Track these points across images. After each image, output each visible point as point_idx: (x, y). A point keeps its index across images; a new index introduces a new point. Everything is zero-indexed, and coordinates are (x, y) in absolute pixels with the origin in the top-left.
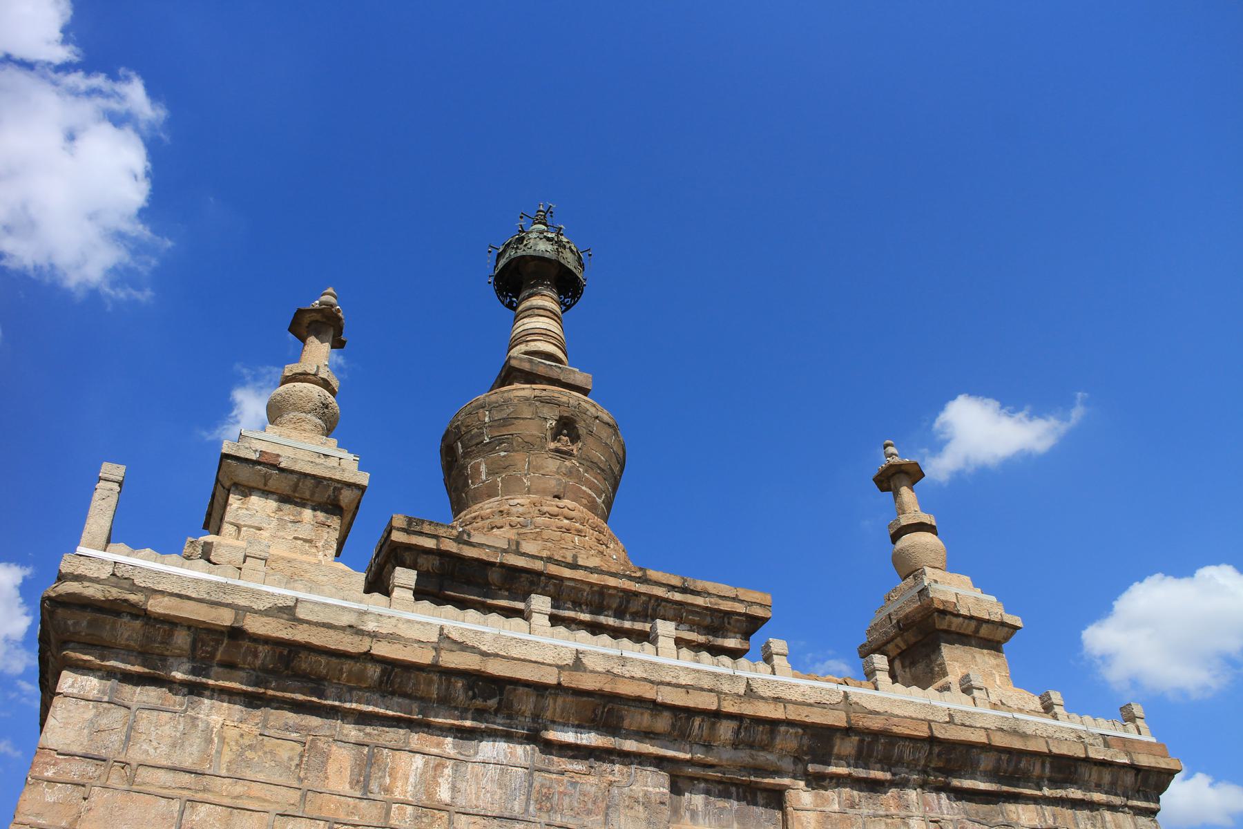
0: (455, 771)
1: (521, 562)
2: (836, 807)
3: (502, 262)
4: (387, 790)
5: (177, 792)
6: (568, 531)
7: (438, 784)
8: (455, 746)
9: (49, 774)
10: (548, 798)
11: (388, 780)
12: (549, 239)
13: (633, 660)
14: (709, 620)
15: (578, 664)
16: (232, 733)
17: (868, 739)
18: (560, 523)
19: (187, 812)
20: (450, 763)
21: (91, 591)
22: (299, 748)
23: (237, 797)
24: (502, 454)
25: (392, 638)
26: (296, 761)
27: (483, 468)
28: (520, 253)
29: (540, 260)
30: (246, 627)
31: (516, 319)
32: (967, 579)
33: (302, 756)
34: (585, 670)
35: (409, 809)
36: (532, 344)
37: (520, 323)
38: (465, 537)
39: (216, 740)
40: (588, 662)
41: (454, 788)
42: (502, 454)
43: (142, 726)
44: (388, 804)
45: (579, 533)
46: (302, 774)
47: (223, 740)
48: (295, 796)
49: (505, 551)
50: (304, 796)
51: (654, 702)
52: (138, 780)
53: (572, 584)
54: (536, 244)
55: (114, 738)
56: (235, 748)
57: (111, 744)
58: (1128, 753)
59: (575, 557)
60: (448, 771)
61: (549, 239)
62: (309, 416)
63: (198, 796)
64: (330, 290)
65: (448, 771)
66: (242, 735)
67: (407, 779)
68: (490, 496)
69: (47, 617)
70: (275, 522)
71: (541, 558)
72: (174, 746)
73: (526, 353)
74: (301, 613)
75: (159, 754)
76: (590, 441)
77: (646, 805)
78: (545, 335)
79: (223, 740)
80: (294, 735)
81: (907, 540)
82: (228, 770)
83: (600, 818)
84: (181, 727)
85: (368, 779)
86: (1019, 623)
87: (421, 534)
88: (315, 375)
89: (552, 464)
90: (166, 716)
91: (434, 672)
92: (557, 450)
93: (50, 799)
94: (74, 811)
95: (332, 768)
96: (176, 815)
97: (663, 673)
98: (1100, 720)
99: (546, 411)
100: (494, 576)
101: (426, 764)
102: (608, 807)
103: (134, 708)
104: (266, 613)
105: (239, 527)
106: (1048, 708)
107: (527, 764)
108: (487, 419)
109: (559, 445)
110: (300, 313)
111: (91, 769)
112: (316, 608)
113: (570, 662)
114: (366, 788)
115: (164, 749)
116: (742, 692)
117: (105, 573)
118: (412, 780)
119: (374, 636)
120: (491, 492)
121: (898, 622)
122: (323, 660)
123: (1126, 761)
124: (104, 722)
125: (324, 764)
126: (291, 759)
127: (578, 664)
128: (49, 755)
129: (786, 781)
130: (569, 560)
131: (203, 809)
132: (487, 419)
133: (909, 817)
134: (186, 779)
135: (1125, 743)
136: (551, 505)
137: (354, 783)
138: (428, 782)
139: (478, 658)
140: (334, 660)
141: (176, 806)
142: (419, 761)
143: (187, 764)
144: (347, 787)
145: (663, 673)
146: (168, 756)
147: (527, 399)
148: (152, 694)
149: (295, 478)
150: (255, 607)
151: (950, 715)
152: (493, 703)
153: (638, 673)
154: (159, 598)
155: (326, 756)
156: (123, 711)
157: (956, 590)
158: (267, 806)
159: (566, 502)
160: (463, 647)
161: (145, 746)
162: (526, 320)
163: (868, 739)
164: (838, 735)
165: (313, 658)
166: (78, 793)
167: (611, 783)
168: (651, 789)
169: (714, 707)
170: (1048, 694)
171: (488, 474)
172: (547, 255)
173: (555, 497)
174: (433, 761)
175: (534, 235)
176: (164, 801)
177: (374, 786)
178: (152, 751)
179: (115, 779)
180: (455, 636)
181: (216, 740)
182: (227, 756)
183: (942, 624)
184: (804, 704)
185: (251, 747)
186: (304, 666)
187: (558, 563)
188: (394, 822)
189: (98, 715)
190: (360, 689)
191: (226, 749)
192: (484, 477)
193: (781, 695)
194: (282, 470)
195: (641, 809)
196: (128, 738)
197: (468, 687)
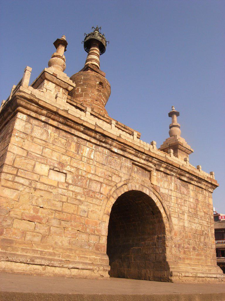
0: (95, 153)
2: (160, 177)
3: (88, 38)
4: (82, 154)
5: (42, 145)
6: (99, 109)
7: (91, 155)
8: (95, 148)
9: (17, 135)
10: (111, 162)
11: (82, 152)
12: (100, 36)
15: (120, 137)
16: (53, 135)
19: (44, 149)
20: (94, 151)
21: (27, 96)
22: (66, 141)
23: (54, 148)
24: (85, 87)
25: (87, 122)
26: (65, 144)
27: (80, 90)
28: (93, 38)
29: (97, 41)
30: (59, 112)
31: (88, 55)
32: (184, 139)
33: (66, 143)
34: (121, 137)
35: (86, 158)
36: (93, 62)
37: (90, 56)
38: (82, 104)
39: (50, 136)
42: (85, 87)
43: (35, 129)
45: (102, 110)
46: (66, 146)
47: (51, 136)
48: (65, 151)
50: (66, 151)
52: (34, 140)
54: (97, 36)
55: (29, 130)
56: (53, 138)
57: (29, 132)
58: (211, 181)
60: (93, 152)
61: (100, 36)
62: (60, 67)
63: (46, 146)
64: (64, 36)
65: (93, 152)
66: (55, 136)
67: (86, 152)
68: (81, 97)
70: (54, 90)
71: (97, 113)
72: (41, 135)
73: (91, 64)
74: (69, 112)
75: (38, 136)
76: (105, 89)
77: (128, 168)
78: (96, 60)
79: (51, 136)
80: (65, 138)
81: (173, 128)
82: (52, 142)
83: (119, 168)
84: (42, 131)
86: (193, 151)
87: (73, 101)
88: (62, 57)
89: (96, 93)
90: (40, 128)
91: (94, 131)
92: (98, 89)
93: (17, 140)
94: (22, 144)
95: (72, 147)
96: (42, 149)
98: (207, 173)
99: (97, 79)
101: (90, 150)
102: (121, 167)
103: (33, 125)
104: (63, 110)
105: (47, 90)
106: (198, 168)
107: (108, 154)
108: (83, 78)
109: (98, 88)
110: (58, 40)
111: (24, 136)
112: (72, 112)
113: (119, 136)
114: (78, 152)
116: (148, 150)
117: (29, 93)
118: (86, 153)
119: (83, 121)
120: (81, 95)
121: (169, 145)
123: (210, 182)
124: (27, 126)
125: (70, 145)
126: (64, 143)
127: (120, 137)
128: (16, 131)
129: (152, 169)
130: (103, 115)
131: (47, 149)
132: (83, 78)
133: (172, 182)
134: (44, 142)
135: (210, 179)
136: (95, 102)
137: (76, 151)
138: (90, 154)
139: (103, 130)
141: (42, 148)
142: (88, 149)
143: (44, 139)
144: (75, 151)
147: (93, 75)
148: (37, 122)
150: (60, 108)
151: (183, 165)
154: (41, 102)
155: (71, 144)
156: (31, 125)
157: (182, 140)
158: (60, 152)
159: (98, 102)
160: (100, 127)
161: (35, 134)
162: (92, 55)
166: (22, 141)
167: (122, 162)
168: (129, 165)
169: (143, 152)
170: (199, 166)
172: (99, 40)
173: (96, 100)
174: (91, 150)
175: (97, 34)
176: (39, 146)
177: (80, 152)
178: (37, 135)
179: (29, 139)
180: (98, 124)
181: (50, 136)
182: (51, 140)
184: (188, 149)
185: (56, 139)
187: (101, 115)
188: (3, 176)
191: (51, 138)
192: (80, 92)
193: (155, 152)
195: (127, 168)
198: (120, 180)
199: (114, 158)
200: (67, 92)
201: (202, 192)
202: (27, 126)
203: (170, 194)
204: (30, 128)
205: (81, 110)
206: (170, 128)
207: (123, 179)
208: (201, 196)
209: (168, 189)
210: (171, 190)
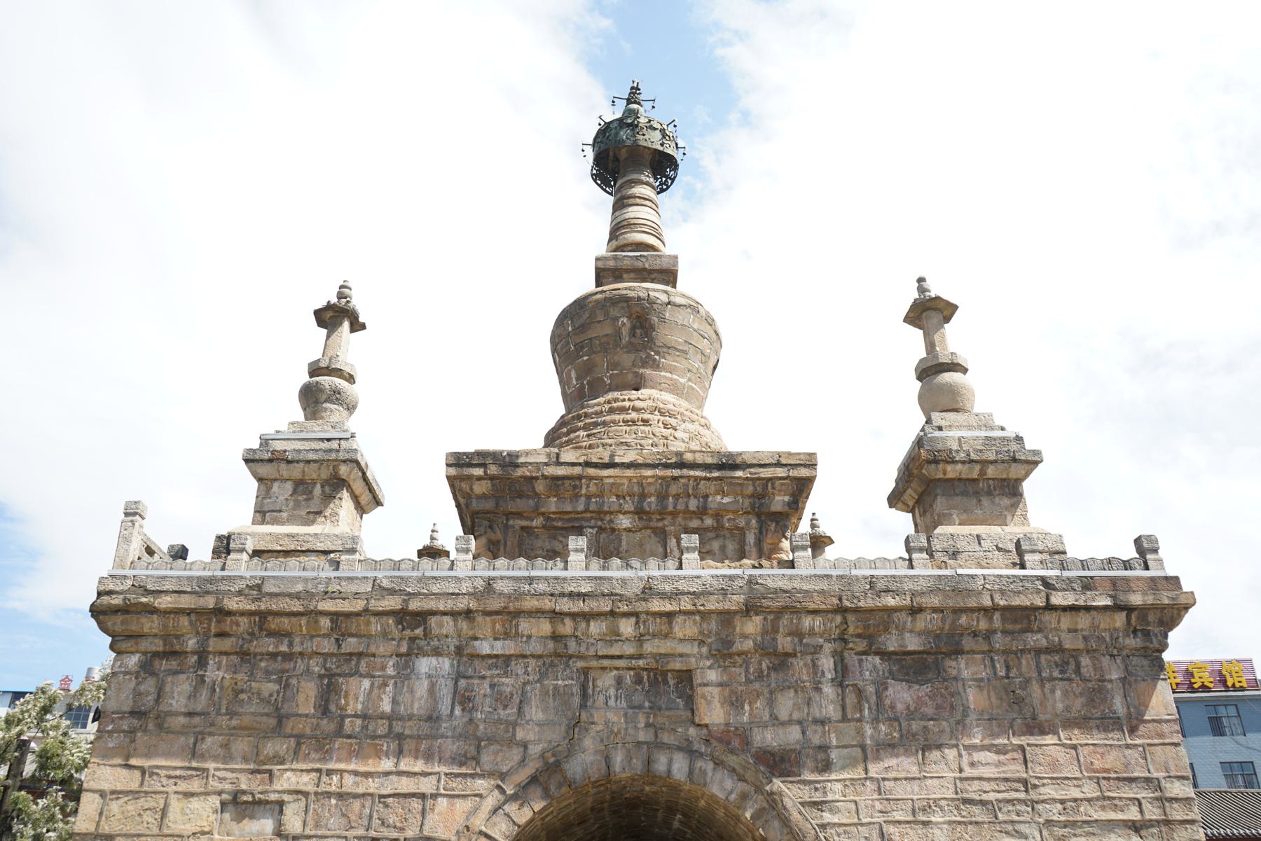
1: (561, 471)
13: (539, 578)
14: (751, 488)
17: (770, 617)
18: (628, 417)
22: (277, 687)
40: (499, 586)
41: (394, 702)
44: (343, 718)
45: (646, 422)
48: (273, 722)
49: (546, 464)
51: (554, 611)
53: (611, 480)
59: (612, 456)
60: (390, 689)
65: (390, 689)
69: (462, 500)
70: (292, 503)
71: (580, 464)
85: (327, 701)
93: (110, 745)
97: (566, 586)
100: (540, 487)
115: (183, 701)
118: (361, 699)
122: (285, 620)
124: (142, 688)
126: (271, 695)
130: (606, 460)
131: (209, 740)
140: (294, 619)
145: (566, 586)
146: (186, 706)
149: (301, 465)
152: (419, 631)
153: (542, 587)
163: (770, 617)
164: (738, 617)
165: (278, 620)
171: (577, 379)
177: (333, 708)
183: (936, 472)
186: (273, 627)
187: (596, 466)
189: (138, 684)
190: (319, 636)
194: (289, 462)
196: (159, 696)
197: (399, 622)
198: (517, 758)
199: (484, 677)
200: (937, 337)
201: (1062, 672)
202: (142, 688)
203: (816, 740)
204: (152, 690)
205: (956, 410)
206: (421, 554)
207: (535, 750)
208: (1058, 693)
209: (800, 722)
210: (822, 722)
